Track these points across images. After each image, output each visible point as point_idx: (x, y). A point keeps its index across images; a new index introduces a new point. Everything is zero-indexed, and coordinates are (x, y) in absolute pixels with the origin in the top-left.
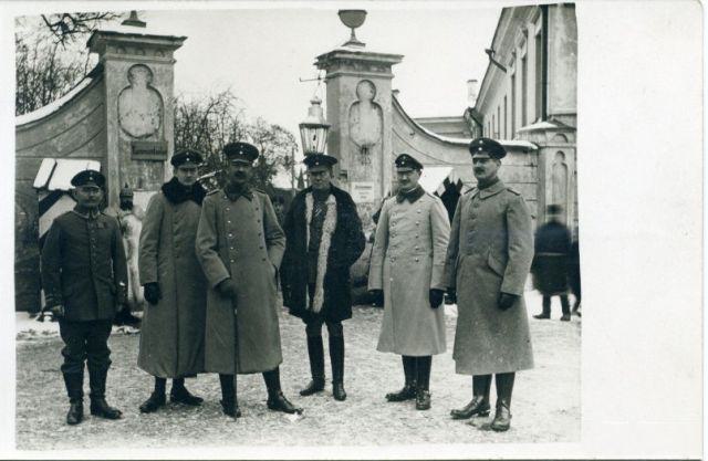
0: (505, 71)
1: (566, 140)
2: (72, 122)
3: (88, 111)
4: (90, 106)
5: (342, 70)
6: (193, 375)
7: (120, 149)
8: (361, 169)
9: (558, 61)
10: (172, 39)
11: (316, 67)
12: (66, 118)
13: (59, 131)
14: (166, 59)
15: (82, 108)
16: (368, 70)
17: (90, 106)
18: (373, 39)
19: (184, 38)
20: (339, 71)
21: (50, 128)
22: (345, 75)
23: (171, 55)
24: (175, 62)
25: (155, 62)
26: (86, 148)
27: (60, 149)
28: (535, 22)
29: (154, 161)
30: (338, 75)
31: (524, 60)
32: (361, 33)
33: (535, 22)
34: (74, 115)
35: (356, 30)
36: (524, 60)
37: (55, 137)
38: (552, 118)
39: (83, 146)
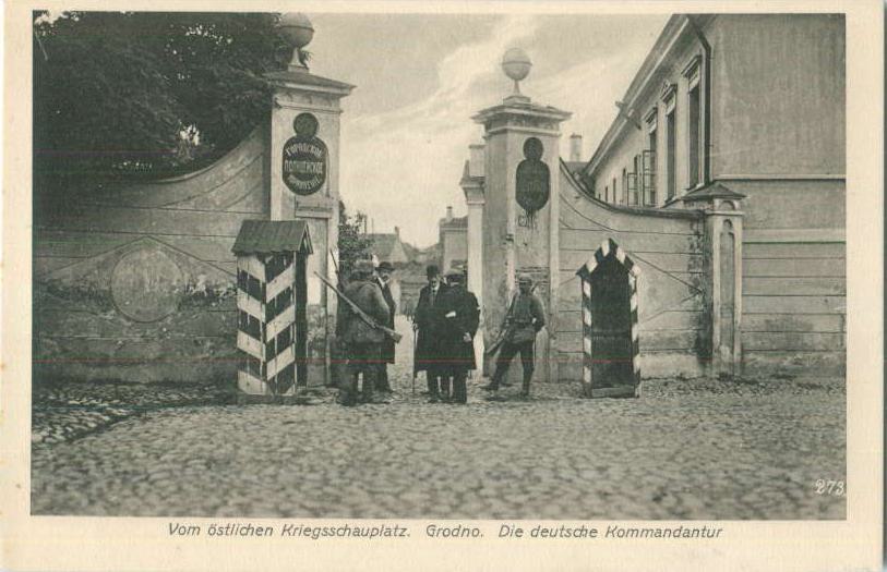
0: (640, 128)
1: (734, 208)
2: (232, 172)
3: (248, 162)
4: (249, 157)
5: (510, 126)
6: (633, 317)
7: (284, 204)
8: (526, 233)
9: (723, 121)
10: (340, 86)
11: (472, 121)
12: (226, 168)
13: (218, 183)
14: (333, 108)
15: (240, 160)
16: (536, 125)
17: (249, 157)
18: (539, 92)
19: (353, 87)
20: (505, 127)
21: (208, 179)
22: (512, 131)
23: (338, 105)
24: (341, 112)
25: (322, 111)
26: (244, 202)
27: (218, 203)
28: (689, 75)
29: (318, 219)
30: (505, 131)
31: (672, 117)
32: (525, 88)
33: (689, 75)
34: (232, 167)
35: (520, 83)
36: (672, 117)
37: (213, 189)
38: (717, 184)
39: (240, 200)
